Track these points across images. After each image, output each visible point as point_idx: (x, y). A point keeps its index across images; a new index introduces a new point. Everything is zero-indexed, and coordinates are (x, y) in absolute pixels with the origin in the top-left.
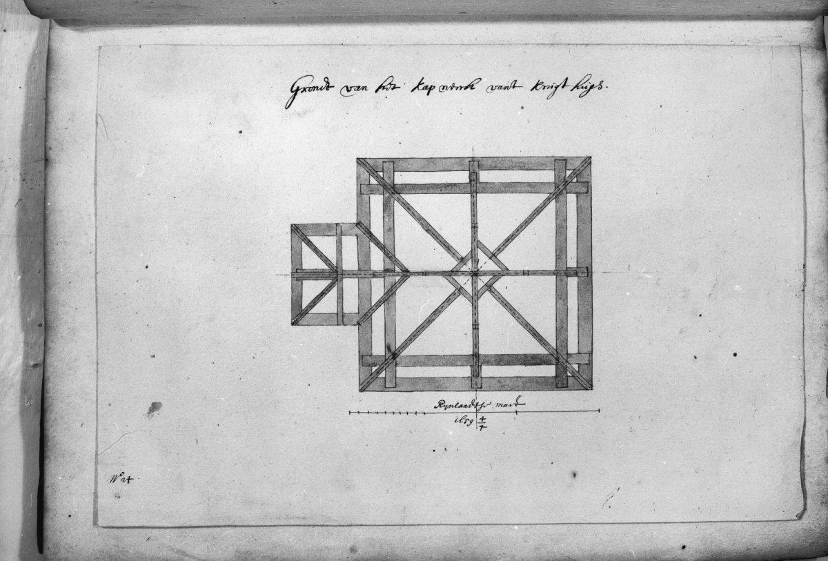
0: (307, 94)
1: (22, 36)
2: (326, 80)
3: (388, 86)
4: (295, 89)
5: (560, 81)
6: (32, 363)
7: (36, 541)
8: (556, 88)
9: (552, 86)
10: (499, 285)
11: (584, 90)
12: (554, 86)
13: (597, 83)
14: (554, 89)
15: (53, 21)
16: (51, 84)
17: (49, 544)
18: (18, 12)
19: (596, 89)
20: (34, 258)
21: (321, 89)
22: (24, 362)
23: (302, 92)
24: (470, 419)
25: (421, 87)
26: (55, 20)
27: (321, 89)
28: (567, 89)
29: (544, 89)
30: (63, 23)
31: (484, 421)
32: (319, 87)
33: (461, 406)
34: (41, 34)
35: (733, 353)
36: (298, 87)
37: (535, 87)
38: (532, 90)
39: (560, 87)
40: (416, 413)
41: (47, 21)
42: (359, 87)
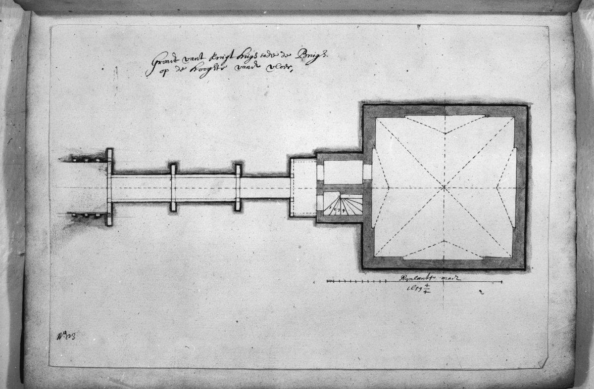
1: (13, 20)
2: (269, 52)
5: (229, 54)
6: (20, 253)
7: (19, 376)
8: (227, 58)
10: (243, 181)
11: (247, 59)
12: (250, 56)
15: (33, 13)
17: (27, 378)
18: (10, 6)
20: (21, 180)
24: (419, 287)
25: (214, 58)
26: (35, 12)
30: (39, 13)
31: (428, 287)
32: (170, 61)
33: (419, 278)
34: (24, 20)
39: (229, 58)
41: (28, 13)
42: (193, 58)
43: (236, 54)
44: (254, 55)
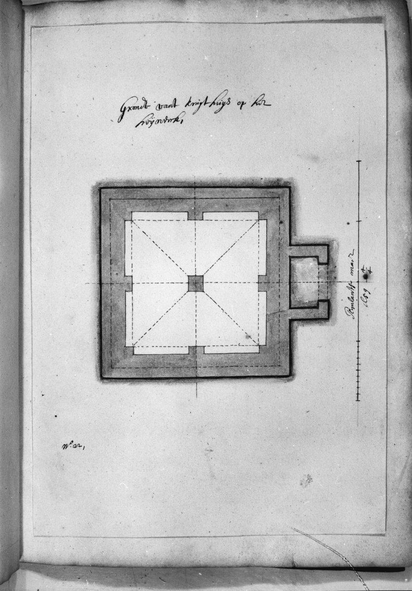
0: (132, 111)
3: (260, 102)
4: (123, 110)
8: (201, 104)
9: (220, 103)
13: (226, 101)
14: (199, 105)
16: (234, 186)
19: (226, 106)
21: (141, 108)
22: (74, 581)
23: (128, 111)
26: (20, 559)
27: (141, 108)
28: (208, 105)
29: (193, 105)
35: (346, 223)
36: (125, 108)
37: (188, 104)
38: (186, 106)
39: (203, 104)
40: (358, 341)
43: (210, 100)
44: (226, 101)
